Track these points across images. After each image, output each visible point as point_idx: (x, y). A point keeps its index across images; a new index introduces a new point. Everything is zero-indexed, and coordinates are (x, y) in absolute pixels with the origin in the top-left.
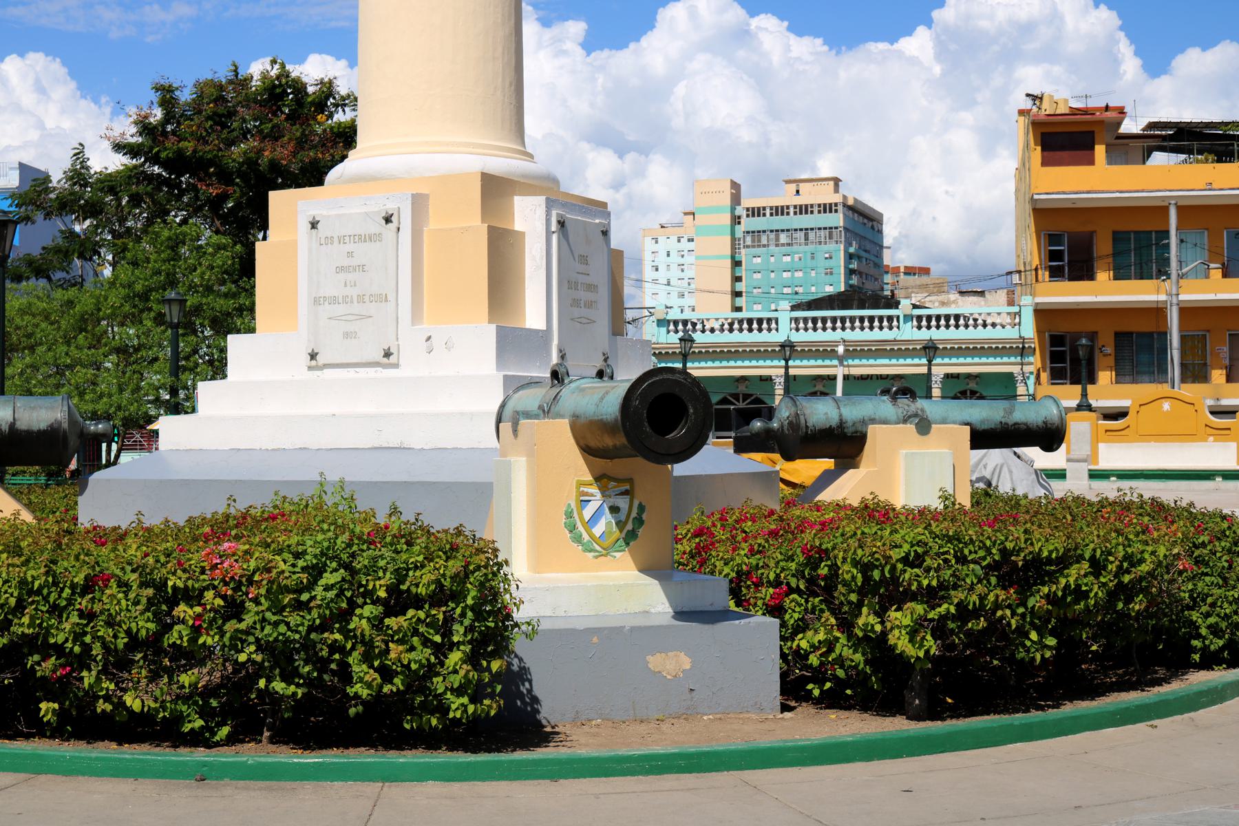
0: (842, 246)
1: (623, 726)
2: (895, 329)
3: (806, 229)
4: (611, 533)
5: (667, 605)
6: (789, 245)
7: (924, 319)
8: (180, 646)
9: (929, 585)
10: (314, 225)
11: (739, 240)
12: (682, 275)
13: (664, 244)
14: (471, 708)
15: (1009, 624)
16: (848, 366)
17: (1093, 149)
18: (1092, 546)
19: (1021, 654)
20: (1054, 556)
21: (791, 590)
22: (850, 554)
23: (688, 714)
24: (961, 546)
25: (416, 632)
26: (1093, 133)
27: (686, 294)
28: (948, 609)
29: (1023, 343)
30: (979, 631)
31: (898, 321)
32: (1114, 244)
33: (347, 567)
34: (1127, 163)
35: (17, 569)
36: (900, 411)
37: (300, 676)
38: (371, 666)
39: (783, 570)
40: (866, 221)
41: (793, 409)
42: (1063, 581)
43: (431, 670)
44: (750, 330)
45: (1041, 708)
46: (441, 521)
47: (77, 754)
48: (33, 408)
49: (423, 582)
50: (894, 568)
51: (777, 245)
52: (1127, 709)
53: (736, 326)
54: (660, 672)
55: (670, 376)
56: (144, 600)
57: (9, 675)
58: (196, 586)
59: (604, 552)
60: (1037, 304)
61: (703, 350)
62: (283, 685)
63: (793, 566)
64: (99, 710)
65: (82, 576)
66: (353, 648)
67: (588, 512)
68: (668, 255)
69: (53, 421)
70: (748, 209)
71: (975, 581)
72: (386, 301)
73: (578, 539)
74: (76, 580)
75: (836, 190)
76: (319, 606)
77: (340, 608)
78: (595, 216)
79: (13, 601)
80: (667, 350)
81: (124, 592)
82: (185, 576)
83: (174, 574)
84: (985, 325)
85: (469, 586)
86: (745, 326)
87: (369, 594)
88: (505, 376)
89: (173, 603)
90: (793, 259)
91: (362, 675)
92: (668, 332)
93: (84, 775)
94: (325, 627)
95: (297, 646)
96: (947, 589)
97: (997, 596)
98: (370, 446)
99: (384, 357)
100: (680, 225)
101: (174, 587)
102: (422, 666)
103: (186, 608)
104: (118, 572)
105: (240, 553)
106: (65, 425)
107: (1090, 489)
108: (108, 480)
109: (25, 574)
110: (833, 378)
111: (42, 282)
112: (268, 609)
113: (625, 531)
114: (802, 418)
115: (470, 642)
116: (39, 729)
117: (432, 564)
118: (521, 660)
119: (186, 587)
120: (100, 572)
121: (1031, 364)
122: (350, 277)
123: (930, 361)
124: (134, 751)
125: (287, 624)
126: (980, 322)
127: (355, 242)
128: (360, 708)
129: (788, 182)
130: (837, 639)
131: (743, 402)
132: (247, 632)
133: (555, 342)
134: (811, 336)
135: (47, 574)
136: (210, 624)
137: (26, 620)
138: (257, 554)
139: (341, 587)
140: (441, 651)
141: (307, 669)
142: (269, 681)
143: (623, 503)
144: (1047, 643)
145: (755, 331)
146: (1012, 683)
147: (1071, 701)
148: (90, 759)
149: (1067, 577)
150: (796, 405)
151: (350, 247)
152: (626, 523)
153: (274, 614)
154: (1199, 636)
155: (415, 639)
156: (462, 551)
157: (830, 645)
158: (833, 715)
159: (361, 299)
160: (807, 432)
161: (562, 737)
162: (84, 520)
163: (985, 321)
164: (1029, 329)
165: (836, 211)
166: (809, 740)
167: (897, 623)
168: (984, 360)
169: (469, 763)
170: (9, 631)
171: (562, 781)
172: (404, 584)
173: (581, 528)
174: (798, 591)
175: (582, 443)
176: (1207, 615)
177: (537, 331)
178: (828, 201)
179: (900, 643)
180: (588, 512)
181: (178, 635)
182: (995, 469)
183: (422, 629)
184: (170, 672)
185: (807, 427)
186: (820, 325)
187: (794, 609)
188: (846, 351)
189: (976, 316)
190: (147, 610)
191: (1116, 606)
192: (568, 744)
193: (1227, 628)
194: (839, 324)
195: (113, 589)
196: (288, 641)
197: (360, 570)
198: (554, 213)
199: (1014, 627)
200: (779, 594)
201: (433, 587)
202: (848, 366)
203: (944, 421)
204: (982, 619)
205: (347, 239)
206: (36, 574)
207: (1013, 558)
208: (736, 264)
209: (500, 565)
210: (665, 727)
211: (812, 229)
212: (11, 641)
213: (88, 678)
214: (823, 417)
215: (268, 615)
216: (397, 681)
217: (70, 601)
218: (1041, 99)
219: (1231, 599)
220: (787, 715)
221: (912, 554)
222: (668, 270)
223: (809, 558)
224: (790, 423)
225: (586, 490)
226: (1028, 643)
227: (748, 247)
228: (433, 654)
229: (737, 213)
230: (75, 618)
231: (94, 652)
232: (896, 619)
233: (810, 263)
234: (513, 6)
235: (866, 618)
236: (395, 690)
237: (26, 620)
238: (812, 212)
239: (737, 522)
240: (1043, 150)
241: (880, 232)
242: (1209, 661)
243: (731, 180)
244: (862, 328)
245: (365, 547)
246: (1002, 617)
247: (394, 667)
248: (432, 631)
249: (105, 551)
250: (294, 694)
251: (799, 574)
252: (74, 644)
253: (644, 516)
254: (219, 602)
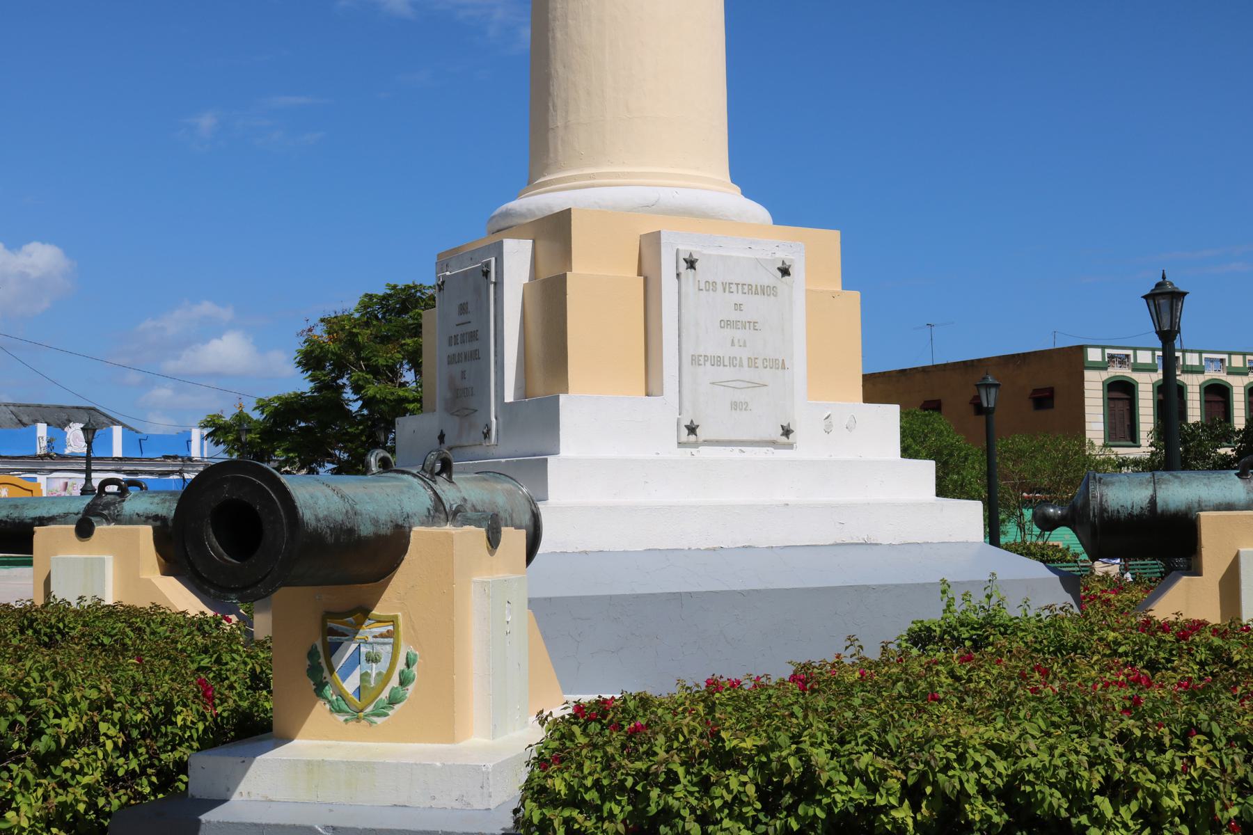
98: (831, 542)
99: (782, 435)
122: (739, 334)
151: (738, 298)
159: (752, 363)
205: (734, 288)
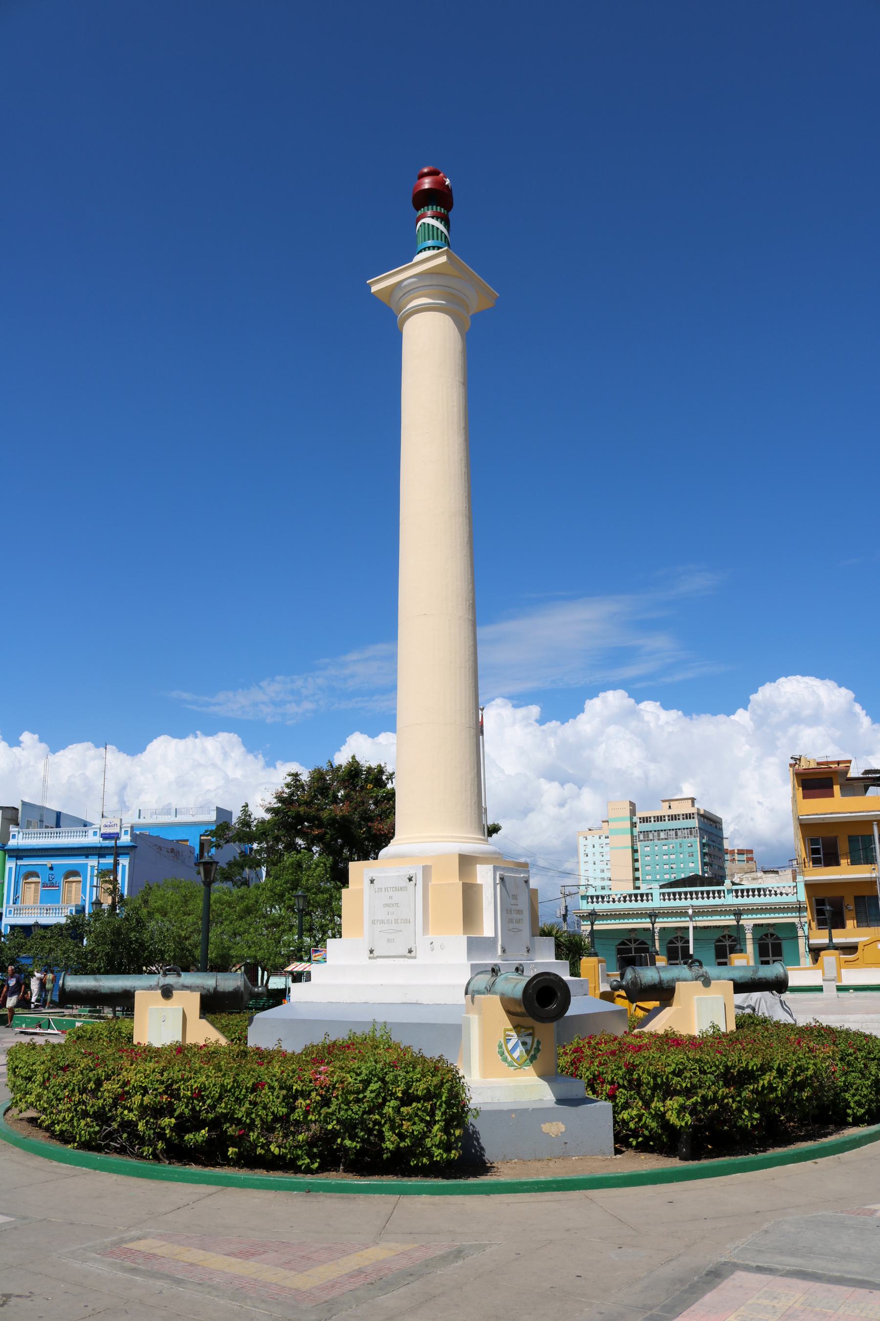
0: (698, 839)
1: (529, 1163)
2: (722, 898)
3: (676, 829)
4: (523, 1056)
5: (553, 1096)
6: (666, 839)
7: (740, 891)
8: (299, 1120)
9: (686, 1086)
10: (372, 881)
11: (636, 837)
12: (602, 859)
13: (591, 840)
14: (445, 1156)
15: (732, 1107)
16: (696, 921)
17: (832, 788)
18: (778, 1062)
19: (740, 1122)
20: (755, 1068)
21: (620, 1086)
22: (646, 1069)
23: (564, 1156)
24: (702, 1065)
25: (417, 1115)
26: (832, 778)
27: (605, 870)
28: (697, 1100)
29: (800, 904)
30: (715, 1111)
31: (724, 893)
32: (849, 843)
33: (382, 1080)
34: (854, 795)
35: (220, 1079)
36: (694, 973)
37: (359, 1138)
38: (394, 1133)
39: (616, 1075)
40: (712, 823)
41: (633, 974)
42: (761, 1082)
43: (424, 1135)
44: (636, 901)
45: (755, 1152)
46: (432, 1053)
47: (247, 1177)
48: (226, 980)
49: (420, 1089)
50: (667, 1078)
51: (659, 840)
52: (800, 1153)
53: (628, 898)
54: (548, 1133)
55: (547, 977)
56: (281, 1097)
57: (214, 1133)
58: (307, 1089)
59: (519, 1067)
60: (806, 881)
61: (609, 913)
62: (350, 1142)
63: (620, 1072)
64: (258, 1153)
65: (251, 1083)
66: (385, 1123)
67: (510, 1045)
68: (594, 847)
69: (236, 986)
70: (640, 818)
71: (711, 1084)
72: (409, 922)
73: (505, 1060)
74: (248, 1085)
75: (693, 805)
76: (368, 1101)
77: (378, 1102)
78: (521, 873)
79: (217, 1095)
81: (272, 1092)
82: (302, 1084)
83: (296, 1083)
84: (776, 894)
85: (444, 1090)
86: (633, 898)
87: (393, 1094)
88: (472, 965)
89: (295, 1098)
90: (669, 847)
91: (389, 1137)
92: (588, 903)
93: (250, 1188)
94: (370, 1112)
95: (357, 1121)
96: (696, 1088)
97: (723, 1092)
100: (600, 828)
101: (296, 1089)
102: (420, 1133)
103: (302, 1101)
104: (269, 1081)
105: (329, 1072)
106: (242, 989)
107: (838, 997)
108: (264, 1018)
109: (224, 1081)
110: (687, 928)
111: (230, 883)
112: (342, 1102)
113: (530, 1055)
114: (638, 979)
115: (444, 1120)
116: (227, 1162)
117: (425, 1079)
118: (474, 1127)
119: (302, 1090)
120: (260, 1081)
121: (805, 917)
124: (275, 1175)
125: (352, 1110)
126: (773, 892)
128: (389, 1154)
129: (663, 801)
130: (643, 1114)
131: (634, 943)
132: (333, 1114)
133: (500, 943)
135: (234, 1082)
136: (314, 1109)
137: (223, 1105)
138: (337, 1073)
139: (379, 1091)
140: (430, 1124)
141: (362, 1134)
142: (343, 1139)
143: (529, 1040)
144: (754, 1116)
145: (639, 901)
146: (738, 1138)
147: (773, 1148)
148: (254, 1179)
149: (763, 1080)
150: (635, 972)
151: (391, 893)
152: (530, 1051)
153: (345, 1105)
154: (850, 1108)
155: (416, 1118)
156: (440, 1071)
157: (640, 1117)
158: (643, 1156)
159: (396, 921)
160: (641, 987)
161: (495, 1170)
162: (252, 1043)
163: (776, 891)
164: (802, 896)
165: (693, 818)
166: (622, 1173)
167: (670, 1107)
168: (777, 915)
169: (444, 1185)
170: (215, 1111)
171: (492, 1195)
172: (410, 1089)
173: (506, 1054)
174: (624, 1087)
175: (506, 1009)
176: (854, 1095)
177: (489, 938)
178: (688, 812)
179: (672, 1119)
180: (510, 1045)
181: (297, 1115)
182: (756, 1001)
183: (420, 1113)
184: (294, 1134)
185: (641, 984)
186: (677, 896)
187: (622, 1095)
188: (694, 912)
189: (770, 889)
190: (283, 1101)
191: (794, 1094)
192: (498, 1174)
193: (866, 1102)
194: (689, 896)
195: (266, 1090)
196: (352, 1118)
197: (389, 1082)
198: (498, 874)
199: (734, 1108)
200: (613, 1089)
201: (425, 1091)
202: (696, 921)
203: (718, 979)
204: (716, 1104)
206: (228, 1081)
207: (732, 1071)
208: (635, 851)
209: (460, 1078)
210: (551, 1164)
211: (679, 829)
212: (216, 1115)
213: (253, 1136)
214: (650, 978)
215: (342, 1105)
216: (407, 1140)
217: (245, 1097)
218: (800, 760)
219: (867, 1086)
220: (619, 1156)
221: (677, 1069)
222: (594, 856)
223: (628, 1068)
224: (632, 982)
225: (509, 1033)
226: (744, 1117)
227: (641, 841)
228: (425, 1126)
229: (634, 821)
230: (247, 1105)
231: (256, 1123)
232: (670, 1105)
233: (679, 850)
234: (476, 762)
235: (656, 1104)
236: (406, 1145)
237: (223, 1105)
238: (679, 819)
239: (597, 1044)
240: (803, 789)
241: (721, 829)
242: (858, 1121)
243: (630, 801)
244: (703, 898)
245: (391, 1070)
246: (727, 1103)
247: (406, 1133)
248: (425, 1114)
249: (262, 1068)
250: (356, 1147)
251: (623, 1078)
252: (247, 1118)
253: (540, 1047)
254: (318, 1098)
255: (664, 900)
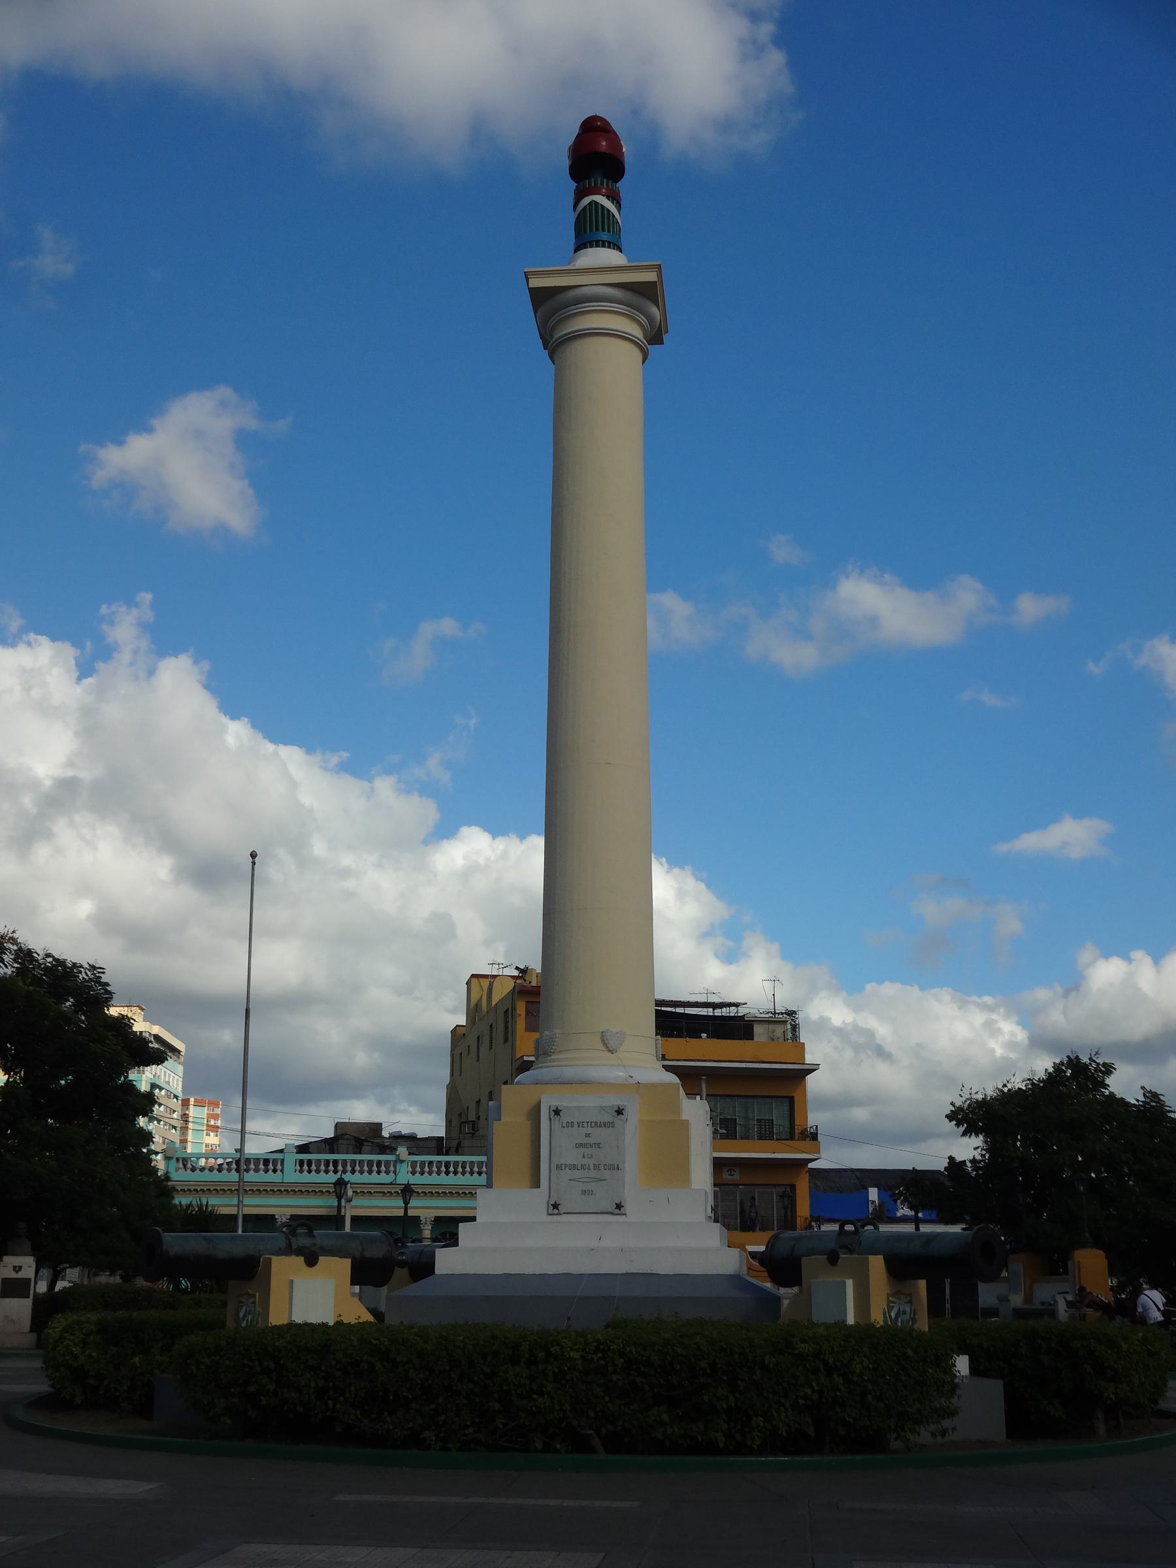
80: (189, 1188)
122: (588, 1151)
123: (406, 1203)
127: (591, 1127)
134: (426, 1179)
151: (589, 1130)
205: (585, 1125)
255: (301, 1171)
